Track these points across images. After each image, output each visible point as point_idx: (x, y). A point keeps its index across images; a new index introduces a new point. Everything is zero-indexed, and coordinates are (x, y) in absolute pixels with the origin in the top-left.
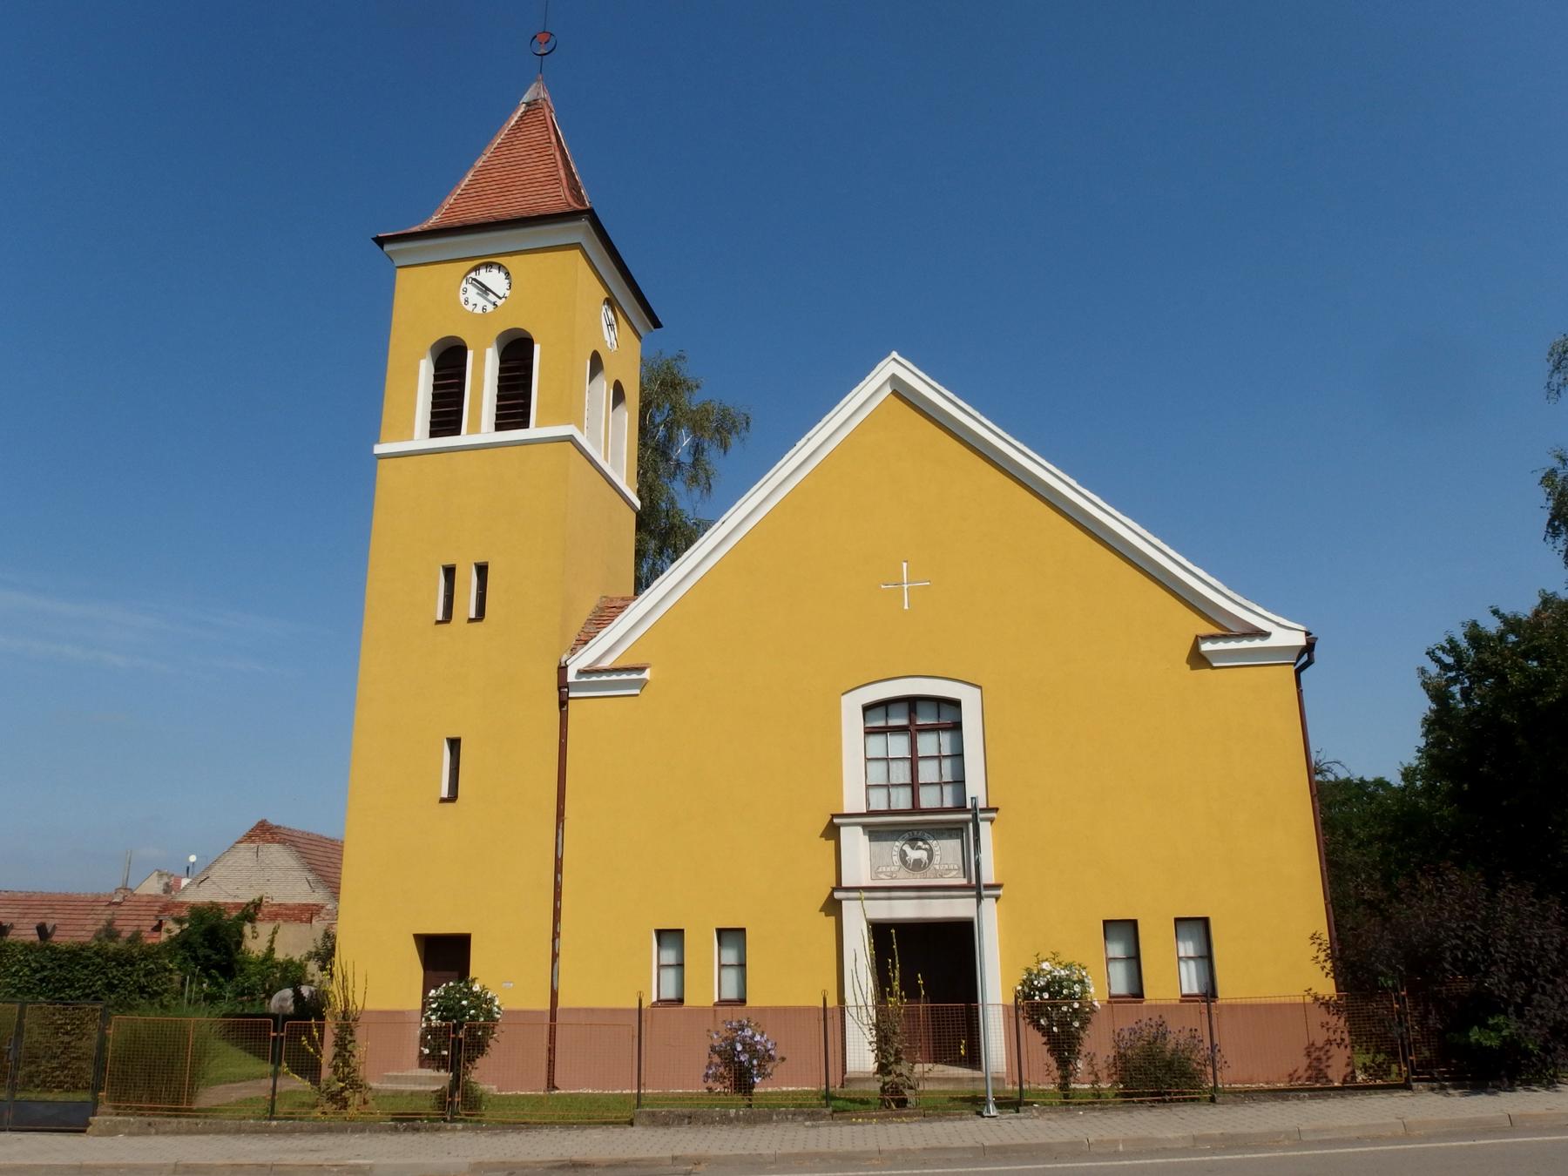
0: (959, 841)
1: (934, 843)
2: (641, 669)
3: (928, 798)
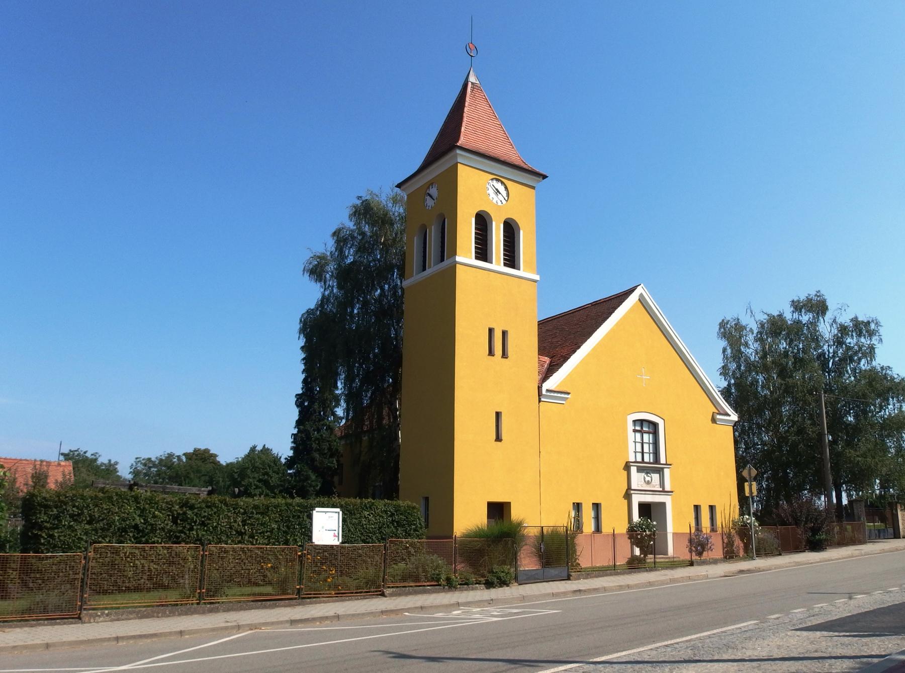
0: (658, 475)
1: (652, 474)
2: (568, 393)
3: (646, 459)
